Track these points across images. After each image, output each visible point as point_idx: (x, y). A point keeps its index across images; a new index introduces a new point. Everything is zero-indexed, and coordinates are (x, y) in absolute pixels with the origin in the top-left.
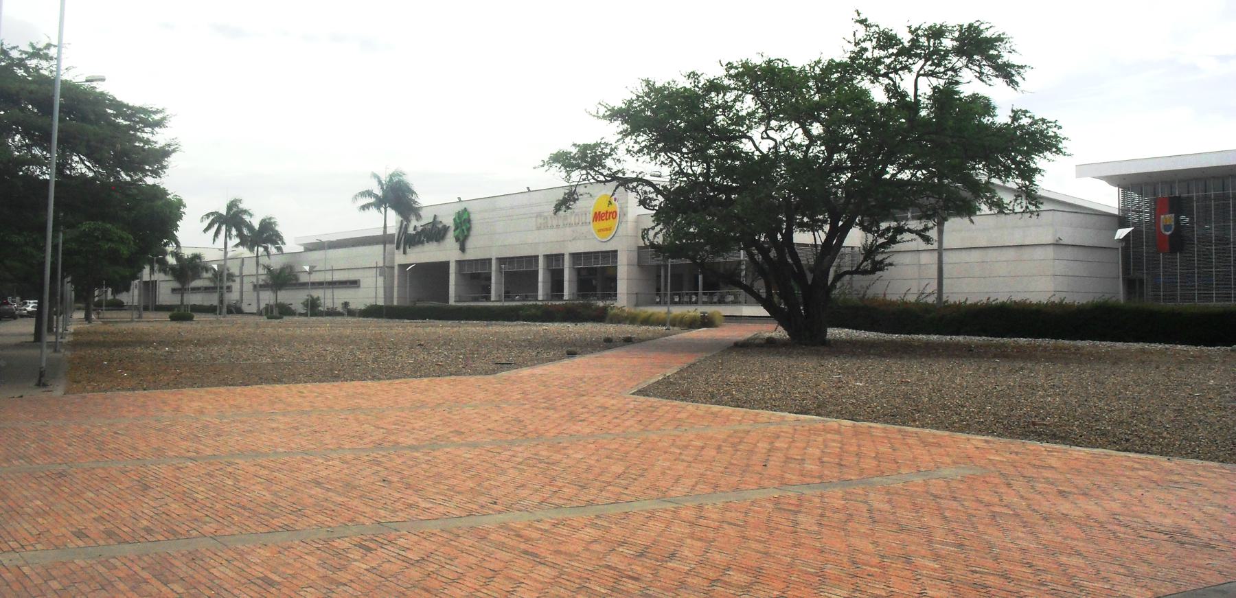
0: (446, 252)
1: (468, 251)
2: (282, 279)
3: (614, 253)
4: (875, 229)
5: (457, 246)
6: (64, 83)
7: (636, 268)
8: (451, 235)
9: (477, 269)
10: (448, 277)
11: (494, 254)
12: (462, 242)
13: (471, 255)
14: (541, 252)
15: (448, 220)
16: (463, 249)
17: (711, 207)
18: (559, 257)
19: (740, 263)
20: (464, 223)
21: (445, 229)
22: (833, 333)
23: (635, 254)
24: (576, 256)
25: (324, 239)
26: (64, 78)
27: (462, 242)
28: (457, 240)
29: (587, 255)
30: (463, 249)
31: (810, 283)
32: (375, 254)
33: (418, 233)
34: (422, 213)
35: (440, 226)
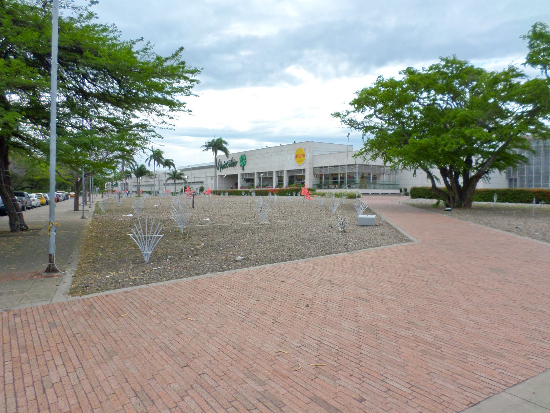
0: (237, 170)
1: (245, 170)
2: (176, 176)
3: (304, 170)
4: (474, 141)
5: (241, 168)
6: (64, 27)
7: (313, 175)
8: (238, 165)
9: (249, 176)
10: (514, 202)
11: (255, 171)
12: (243, 167)
13: (246, 171)
14: (274, 170)
15: (238, 160)
16: (243, 169)
17: (514, 141)
18: (282, 172)
19: (356, 173)
20: (243, 159)
21: (236, 162)
22: (475, 203)
23: (312, 170)
24: (288, 171)
25: (191, 167)
26: (66, 14)
27: (243, 167)
28: (241, 166)
29: (293, 171)
30: (243, 169)
31: (462, 185)
32: (211, 172)
33: (225, 164)
34: (229, 156)
35: (234, 161)
